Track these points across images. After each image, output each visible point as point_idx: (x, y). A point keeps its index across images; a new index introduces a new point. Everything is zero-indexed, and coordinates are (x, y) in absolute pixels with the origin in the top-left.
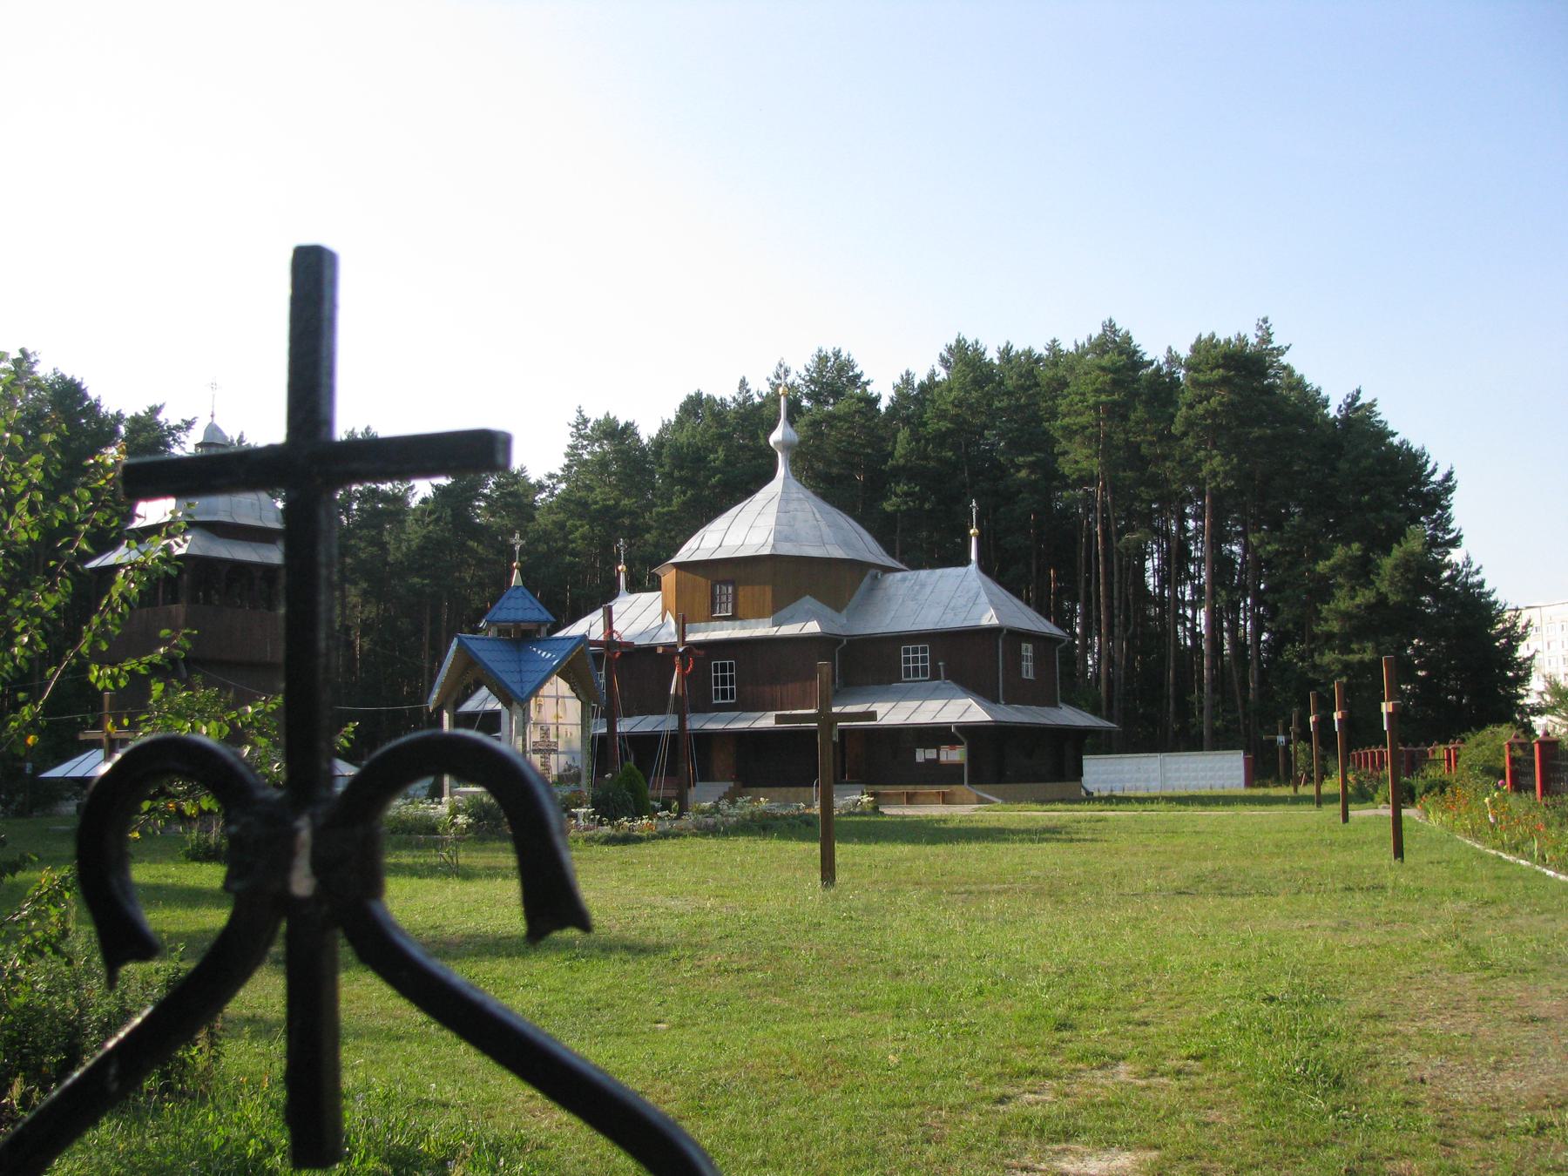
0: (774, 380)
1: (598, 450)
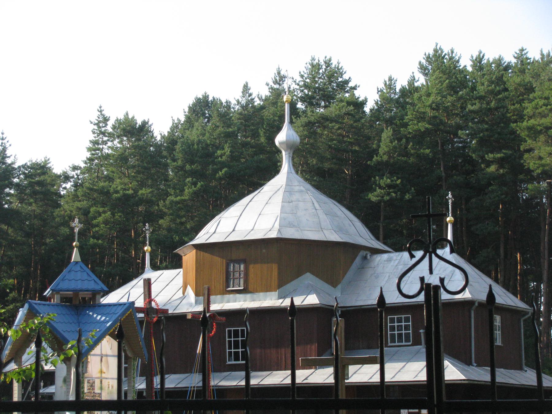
0: (273, 85)
1: (119, 145)
